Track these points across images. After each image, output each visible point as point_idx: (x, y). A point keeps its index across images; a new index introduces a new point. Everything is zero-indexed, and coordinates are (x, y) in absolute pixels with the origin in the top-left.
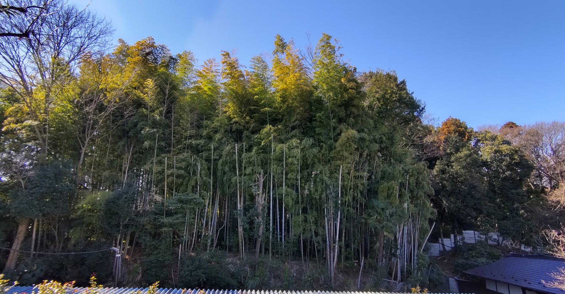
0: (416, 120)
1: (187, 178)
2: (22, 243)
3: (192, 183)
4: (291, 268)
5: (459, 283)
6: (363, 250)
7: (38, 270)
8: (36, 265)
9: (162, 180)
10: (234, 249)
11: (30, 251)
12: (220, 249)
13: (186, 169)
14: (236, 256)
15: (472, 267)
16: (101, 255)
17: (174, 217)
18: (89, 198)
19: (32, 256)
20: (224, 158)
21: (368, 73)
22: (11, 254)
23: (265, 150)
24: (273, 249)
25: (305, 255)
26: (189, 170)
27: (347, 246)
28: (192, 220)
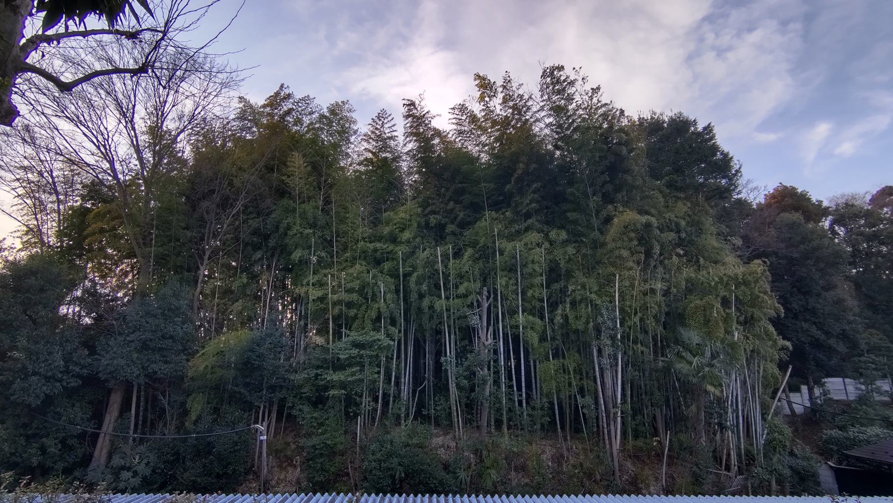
0: (724, 193)
1: (364, 307)
2: (116, 421)
3: (374, 315)
4: (543, 451)
5: (838, 474)
6: (668, 418)
7: (143, 465)
8: (137, 457)
9: (325, 311)
10: (444, 423)
11: (128, 433)
12: (421, 423)
13: (361, 291)
14: (448, 433)
15: (855, 443)
16: (236, 438)
17: (349, 371)
18: (211, 347)
19: (131, 441)
20: (420, 271)
21: (636, 119)
22: (100, 440)
23: (485, 254)
24: (509, 420)
25: (563, 428)
26: (366, 294)
27: (636, 411)
28: (376, 376)
